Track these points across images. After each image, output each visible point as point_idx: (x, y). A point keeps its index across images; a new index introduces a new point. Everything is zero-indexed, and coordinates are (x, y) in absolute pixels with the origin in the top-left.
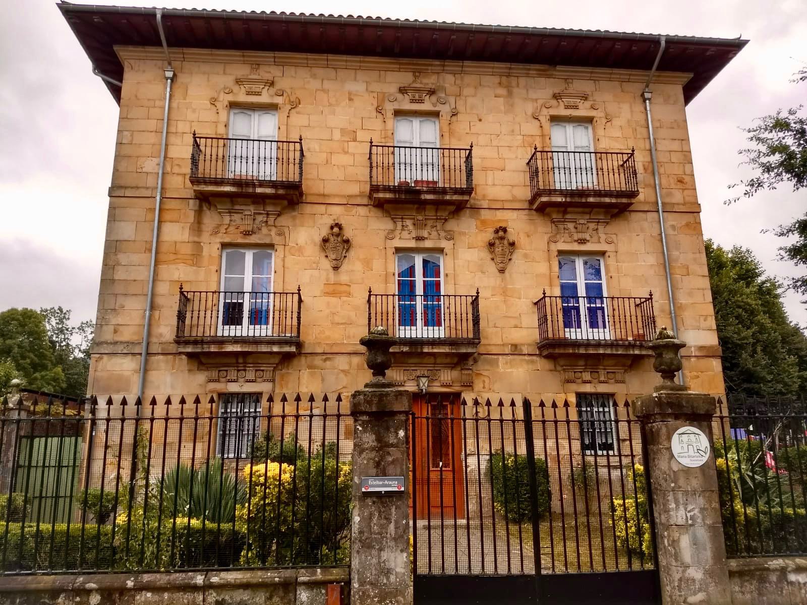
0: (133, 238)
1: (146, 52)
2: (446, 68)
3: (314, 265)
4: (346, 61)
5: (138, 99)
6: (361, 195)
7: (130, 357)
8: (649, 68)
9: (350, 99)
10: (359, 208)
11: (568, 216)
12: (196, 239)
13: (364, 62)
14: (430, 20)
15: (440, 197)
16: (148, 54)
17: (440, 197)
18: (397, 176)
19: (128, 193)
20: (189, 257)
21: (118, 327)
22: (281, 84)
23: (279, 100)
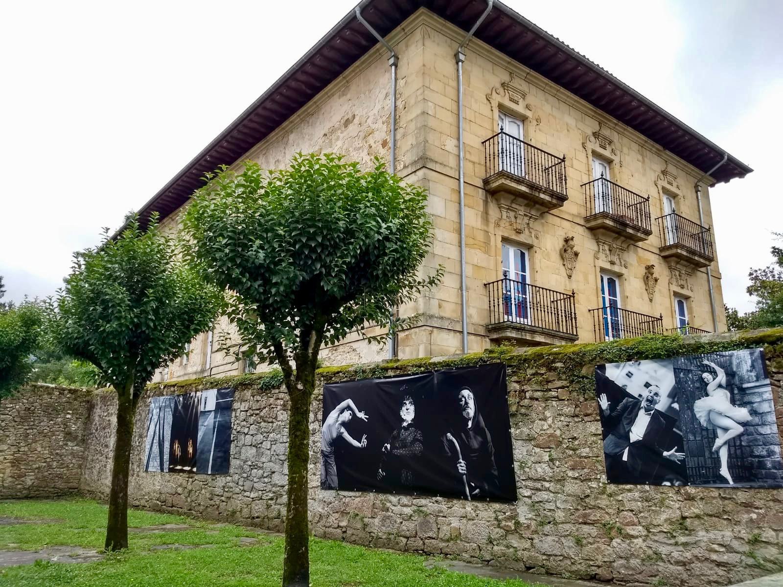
0: (443, 215)
1: (444, 25)
2: (617, 127)
3: (557, 271)
4: (568, 97)
5: (437, 72)
6: (579, 216)
7: (452, 333)
8: (706, 172)
9: (568, 131)
10: (579, 227)
11: (678, 266)
12: (486, 228)
13: (578, 102)
14: (571, 47)
15: (691, 256)
16: (443, 29)
17: (691, 256)
18: (496, 168)
19: (438, 168)
20: (482, 244)
21: (443, 302)
22: (530, 99)
23: (528, 114)
